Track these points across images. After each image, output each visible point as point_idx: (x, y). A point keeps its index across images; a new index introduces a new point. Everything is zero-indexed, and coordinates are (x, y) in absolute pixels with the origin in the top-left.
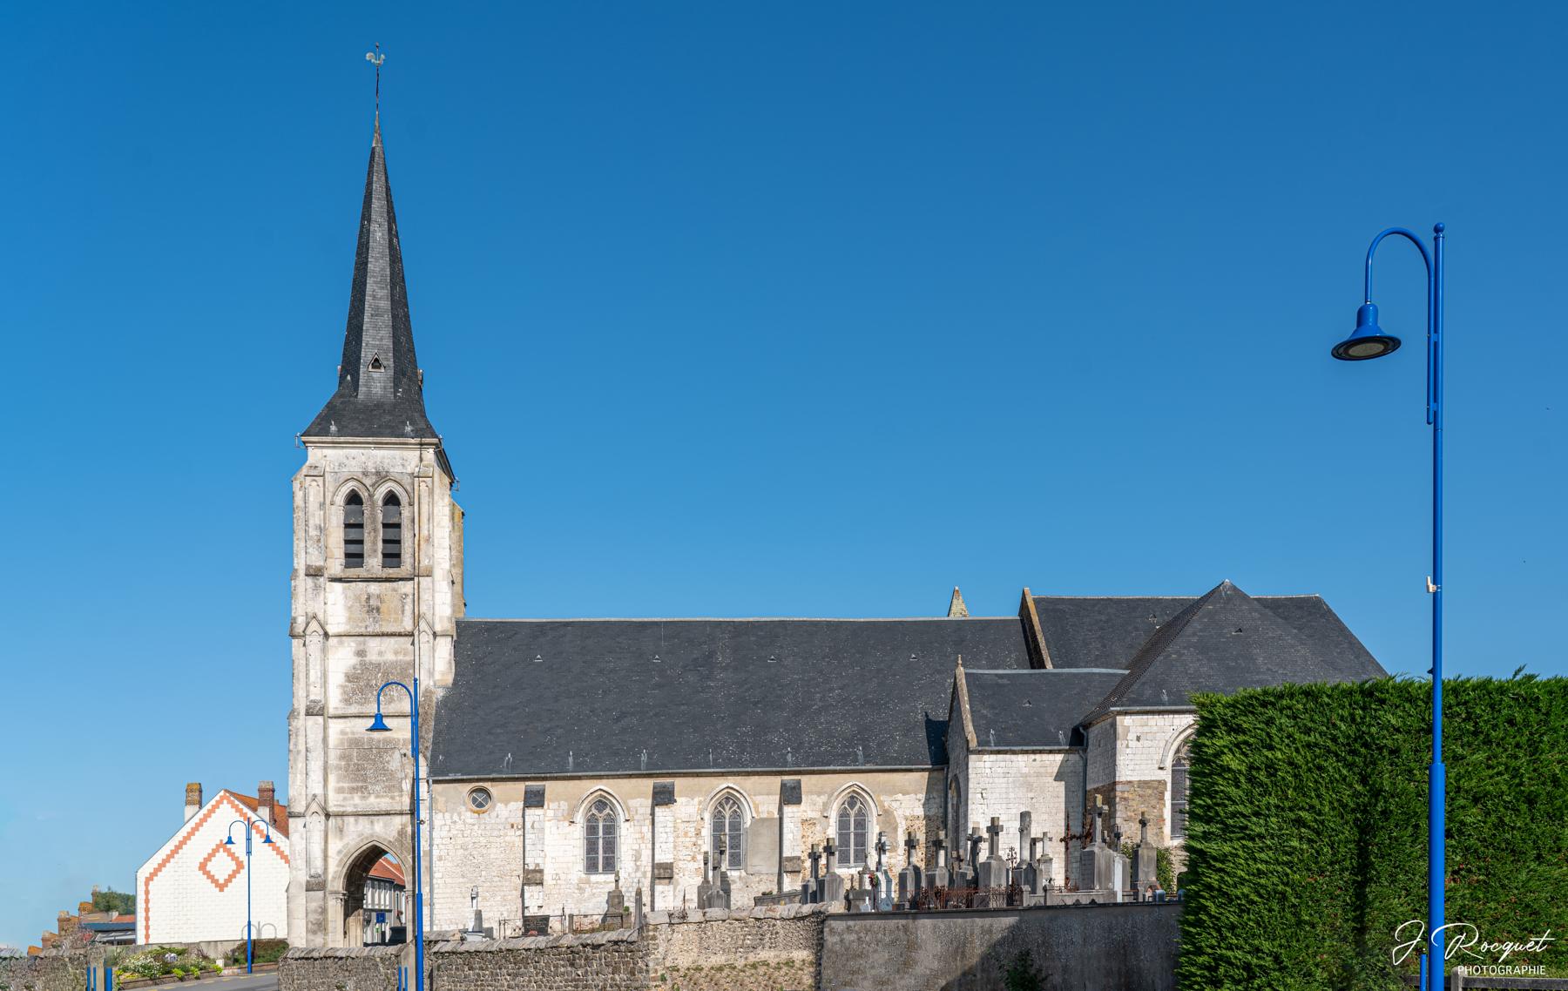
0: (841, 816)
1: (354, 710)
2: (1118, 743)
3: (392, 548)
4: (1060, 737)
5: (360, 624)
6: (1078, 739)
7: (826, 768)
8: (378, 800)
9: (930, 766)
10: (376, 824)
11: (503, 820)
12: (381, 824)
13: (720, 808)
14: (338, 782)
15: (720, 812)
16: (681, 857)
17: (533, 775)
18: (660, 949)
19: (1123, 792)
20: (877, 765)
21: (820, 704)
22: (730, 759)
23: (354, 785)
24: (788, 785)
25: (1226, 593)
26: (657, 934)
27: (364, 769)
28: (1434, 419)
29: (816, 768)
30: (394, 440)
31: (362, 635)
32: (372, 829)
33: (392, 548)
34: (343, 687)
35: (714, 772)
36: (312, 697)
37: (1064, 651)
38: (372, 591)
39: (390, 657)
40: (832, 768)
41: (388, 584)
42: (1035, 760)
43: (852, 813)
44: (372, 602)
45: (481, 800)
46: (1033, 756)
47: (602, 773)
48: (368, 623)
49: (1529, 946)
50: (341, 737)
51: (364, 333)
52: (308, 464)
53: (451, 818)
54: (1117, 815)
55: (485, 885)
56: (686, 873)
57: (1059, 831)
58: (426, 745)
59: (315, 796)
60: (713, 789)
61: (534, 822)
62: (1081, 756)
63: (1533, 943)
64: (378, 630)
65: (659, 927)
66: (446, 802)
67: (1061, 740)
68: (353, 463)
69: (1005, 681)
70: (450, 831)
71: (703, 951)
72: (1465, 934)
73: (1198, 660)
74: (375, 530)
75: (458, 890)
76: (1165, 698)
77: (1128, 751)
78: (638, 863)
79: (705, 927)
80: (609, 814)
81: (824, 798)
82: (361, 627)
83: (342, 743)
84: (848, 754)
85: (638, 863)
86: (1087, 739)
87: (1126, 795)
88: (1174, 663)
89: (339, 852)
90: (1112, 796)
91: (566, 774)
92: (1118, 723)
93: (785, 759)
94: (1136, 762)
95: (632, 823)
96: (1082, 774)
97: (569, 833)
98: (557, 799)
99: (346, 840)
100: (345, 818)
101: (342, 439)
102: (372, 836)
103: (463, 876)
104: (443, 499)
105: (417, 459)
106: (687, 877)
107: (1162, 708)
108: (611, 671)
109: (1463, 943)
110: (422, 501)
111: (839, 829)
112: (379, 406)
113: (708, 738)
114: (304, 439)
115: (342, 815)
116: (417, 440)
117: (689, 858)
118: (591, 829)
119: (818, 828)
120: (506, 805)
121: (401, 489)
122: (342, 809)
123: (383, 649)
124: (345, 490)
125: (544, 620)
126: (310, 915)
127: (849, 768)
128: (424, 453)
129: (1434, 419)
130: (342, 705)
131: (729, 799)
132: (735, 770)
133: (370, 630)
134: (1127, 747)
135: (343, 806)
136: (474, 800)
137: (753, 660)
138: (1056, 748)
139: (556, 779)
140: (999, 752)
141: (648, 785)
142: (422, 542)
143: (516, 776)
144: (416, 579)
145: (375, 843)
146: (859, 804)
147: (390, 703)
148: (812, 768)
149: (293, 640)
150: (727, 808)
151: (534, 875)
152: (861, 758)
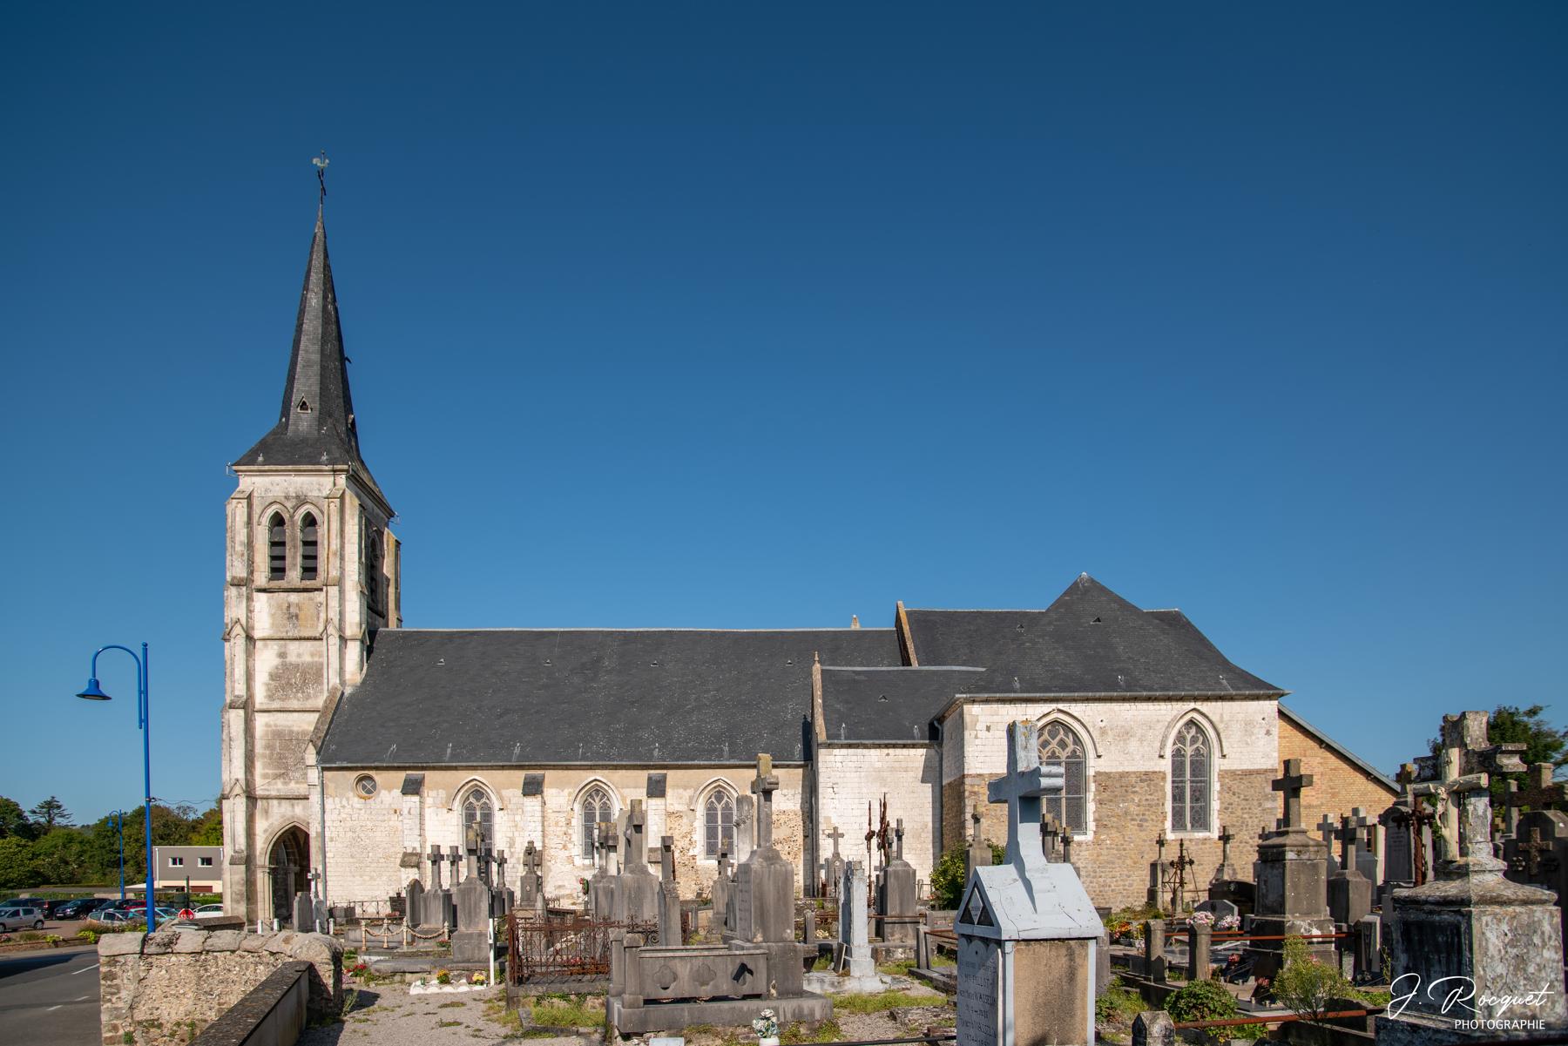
0: (709, 809)
1: (276, 705)
2: (967, 733)
3: (310, 563)
4: (915, 731)
5: (282, 630)
6: (934, 734)
7: (690, 763)
8: (298, 786)
9: (802, 763)
10: (296, 807)
11: (387, 806)
12: (301, 807)
13: (590, 800)
14: (264, 769)
15: (590, 803)
16: (552, 846)
17: (412, 764)
18: (123, 994)
19: (972, 786)
20: (741, 760)
21: (694, 704)
22: (598, 753)
23: (277, 772)
24: (654, 778)
25: (1083, 585)
26: (116, 970)
27: (286, 758)
29: (680, 763)
30: (310, 467)
31: (283, 639)
32: (294, 811)
33: (310, 563)
34: (267, 684)
35: (581, 765)
36: (237, 693)
37: (932, 656)
38: (292, 600)
39: (307, 659)
40: (696, 762)
41: (305, 594)
42: (888, 755)
43: (719, 807)
44: (292, 610)
45: (366, 786)
46: (886, 751)
47: (475, 764)
48: (288, 628)
50: (265, 729)
51: (296, 381)
52: (238, 490)
53: (341, 802)
54: (967, 811)
55: (372, 866)
56: (558, 861)
57: (915, 827)
58: (319, 735)
59: (237, 780)
60: (582, 781)
61: (410, 809)
62: (936, 751)
63: (1532, 996)
64: (297, 634)
65: (122, 959)
66: (336, 788)
67: (915, 734)
68: (278, 488)
69: (862, 678)
70: (339, 814)
71: (203, 998)
72: (1462, 988)
73: (1054, 649)
74: (295, 547)
75: (348, 869)
76: (1017, 685)
77: (977, 742)
78: (512, 850)
79: (206, 960)
80: (485, 803)
81: (690, 792)
82: (282, 632)
83: (266, 734)
84: (715, 750)
85: (512, 850)
86: (942, 734)
87: (976, 789)
88: (1027, 651)
89: (265, 831)
90: (962, 790)
91: (441, 764)
92: (965, 711)
93: (652, 753)
94: (988, 754)
95: (506, 812)
96: (938, 769)
97: (448, 819)
98: (436, 787)
99: (270, 821)
100: (270, 801)
101: (266, 468)
102: (293, 817)
103: (352, 857)
104: (353, 519)
105: (332, 484)
106: (559, 865)
107: (1012, 695)
108: (504, 674)
109: (1459, 997)
110: (331, 519)
111: (707, 822)
112: (304, 441)
113: (581, 733)
114: (235, 468)
115: (267, 798)
116: (330, 467)
117: (561, 846)
118: (470, 817)
119: (685, 820)
120: (390, 791)
121: (317, 511)
122: (267, 793)
123: (301, 651)
124: (270, 512)
125: (455, 630)
126: (233, 887)
127: (713, 763)
128: (338, 478)
130: (266, 701)
131: (596, 791)
132: (601, 763)
133: (290, 634)
134: (976, 737)
135: (268, 790)
136: (364, 787)
137: (638, 664)
138: (909, 742)
139: (434, 768)
140: (850, 746)
141: (520, 776)
142: (330, 556)
143: (396, 765)
144: (325, 588)
145: (295, 824)
146: (726, 798)
147: (307, 699)
148: (693, 763)
149: (226, 644)
150: (597, 799)
151: (411, 857)
152: (726, 754)
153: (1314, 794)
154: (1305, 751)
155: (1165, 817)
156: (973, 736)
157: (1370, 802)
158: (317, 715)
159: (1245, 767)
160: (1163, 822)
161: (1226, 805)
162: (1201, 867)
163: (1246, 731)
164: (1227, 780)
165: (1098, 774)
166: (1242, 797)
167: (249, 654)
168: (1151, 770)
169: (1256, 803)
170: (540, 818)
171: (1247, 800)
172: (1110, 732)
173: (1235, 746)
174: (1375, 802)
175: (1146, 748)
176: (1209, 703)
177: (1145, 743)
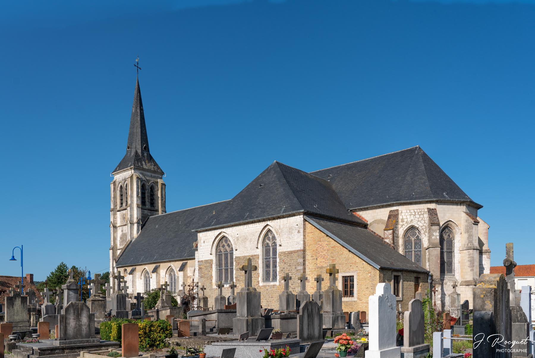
28: (22, 265)
49: (521, 342)
72: (499, 338)
114: (113, 174)
129: (22, 265)
153: (324, 261)
154: (320, 238)
155: (259, 275)
156: (200, 245)
157: (351, 263)
158: (121, 250)
159: (289, 250)
160: (258, 278)
161: (282, 269)
162: (272, 299)
163: (290, 232)
164: (282, 257)
165: (236, 257)
166: (288, 264)
167: (115, 232)
168: (254, 254)
169: (294, 267)
170: (156, 281)
171: (290, 266)
172: (240, 239)
173: (285, 240)
174: (353, 263)
175: (252, 244)
176: (275, 221)
177: (252, 242)
